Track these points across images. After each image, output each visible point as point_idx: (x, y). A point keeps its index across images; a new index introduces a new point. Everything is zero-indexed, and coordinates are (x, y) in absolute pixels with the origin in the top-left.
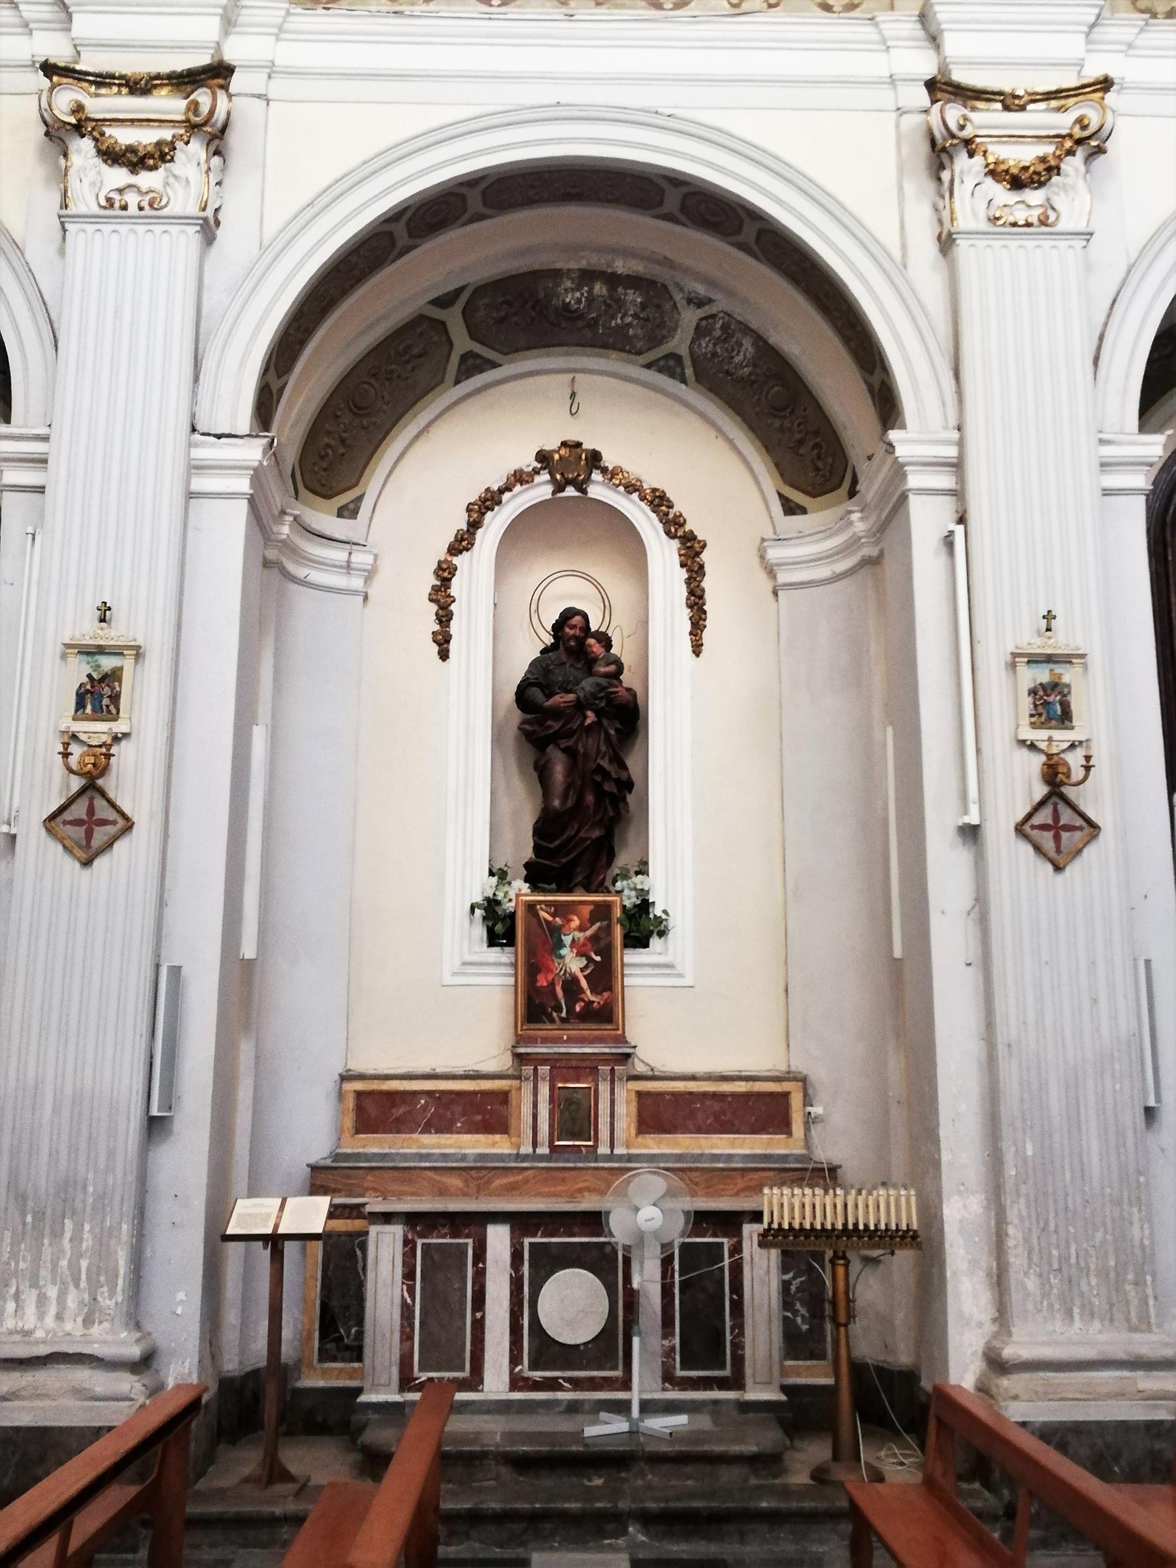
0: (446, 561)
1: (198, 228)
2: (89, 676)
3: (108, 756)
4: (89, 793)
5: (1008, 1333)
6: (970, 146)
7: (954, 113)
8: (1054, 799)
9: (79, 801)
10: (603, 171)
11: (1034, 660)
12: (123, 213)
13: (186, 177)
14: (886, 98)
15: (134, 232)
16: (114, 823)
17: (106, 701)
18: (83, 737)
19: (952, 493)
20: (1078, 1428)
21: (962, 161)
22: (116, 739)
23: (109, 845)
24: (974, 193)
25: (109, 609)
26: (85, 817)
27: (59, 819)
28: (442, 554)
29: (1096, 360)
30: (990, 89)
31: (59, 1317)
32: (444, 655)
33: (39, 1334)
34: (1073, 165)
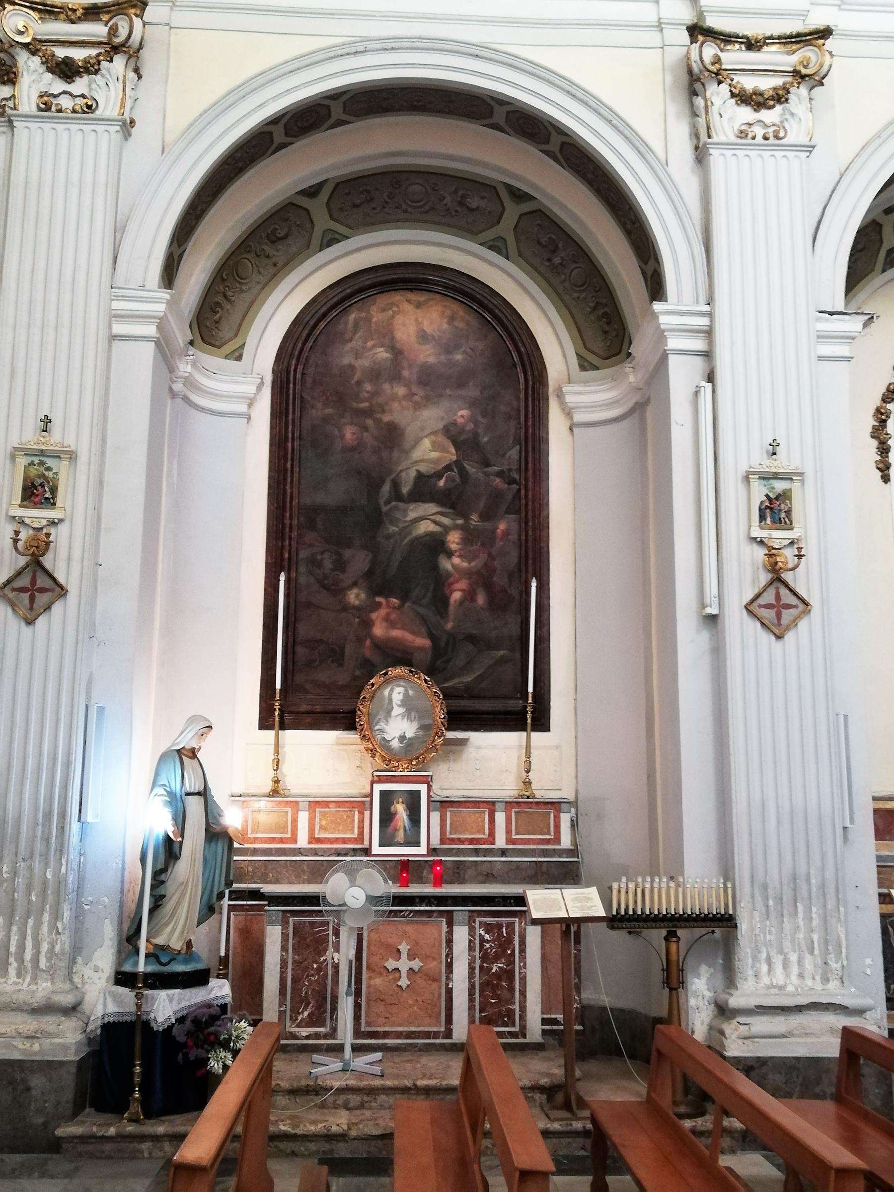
0: (881, 407)
2: (767, 496)
5: (786, 988)
6: (718, 76)
7: (710, 50)
8: (776, 584)
9: (769, 589)
10: (442, 91)
11: (766, 477)
12: (753, 142)
14: (654, 37)
15: (761, 156)
16: (796, 607)
17: (783, 515)
18: (27, 521)
20: (762, 1062)
22: (53, 523)
23: (48, 608)
24: (727, 116)
26: (774, 602)
27: (755, 604)
28: (878, 402)
31: (801, 976)
32: (886, 479)
33: (790, 989)
34: (799, 93)
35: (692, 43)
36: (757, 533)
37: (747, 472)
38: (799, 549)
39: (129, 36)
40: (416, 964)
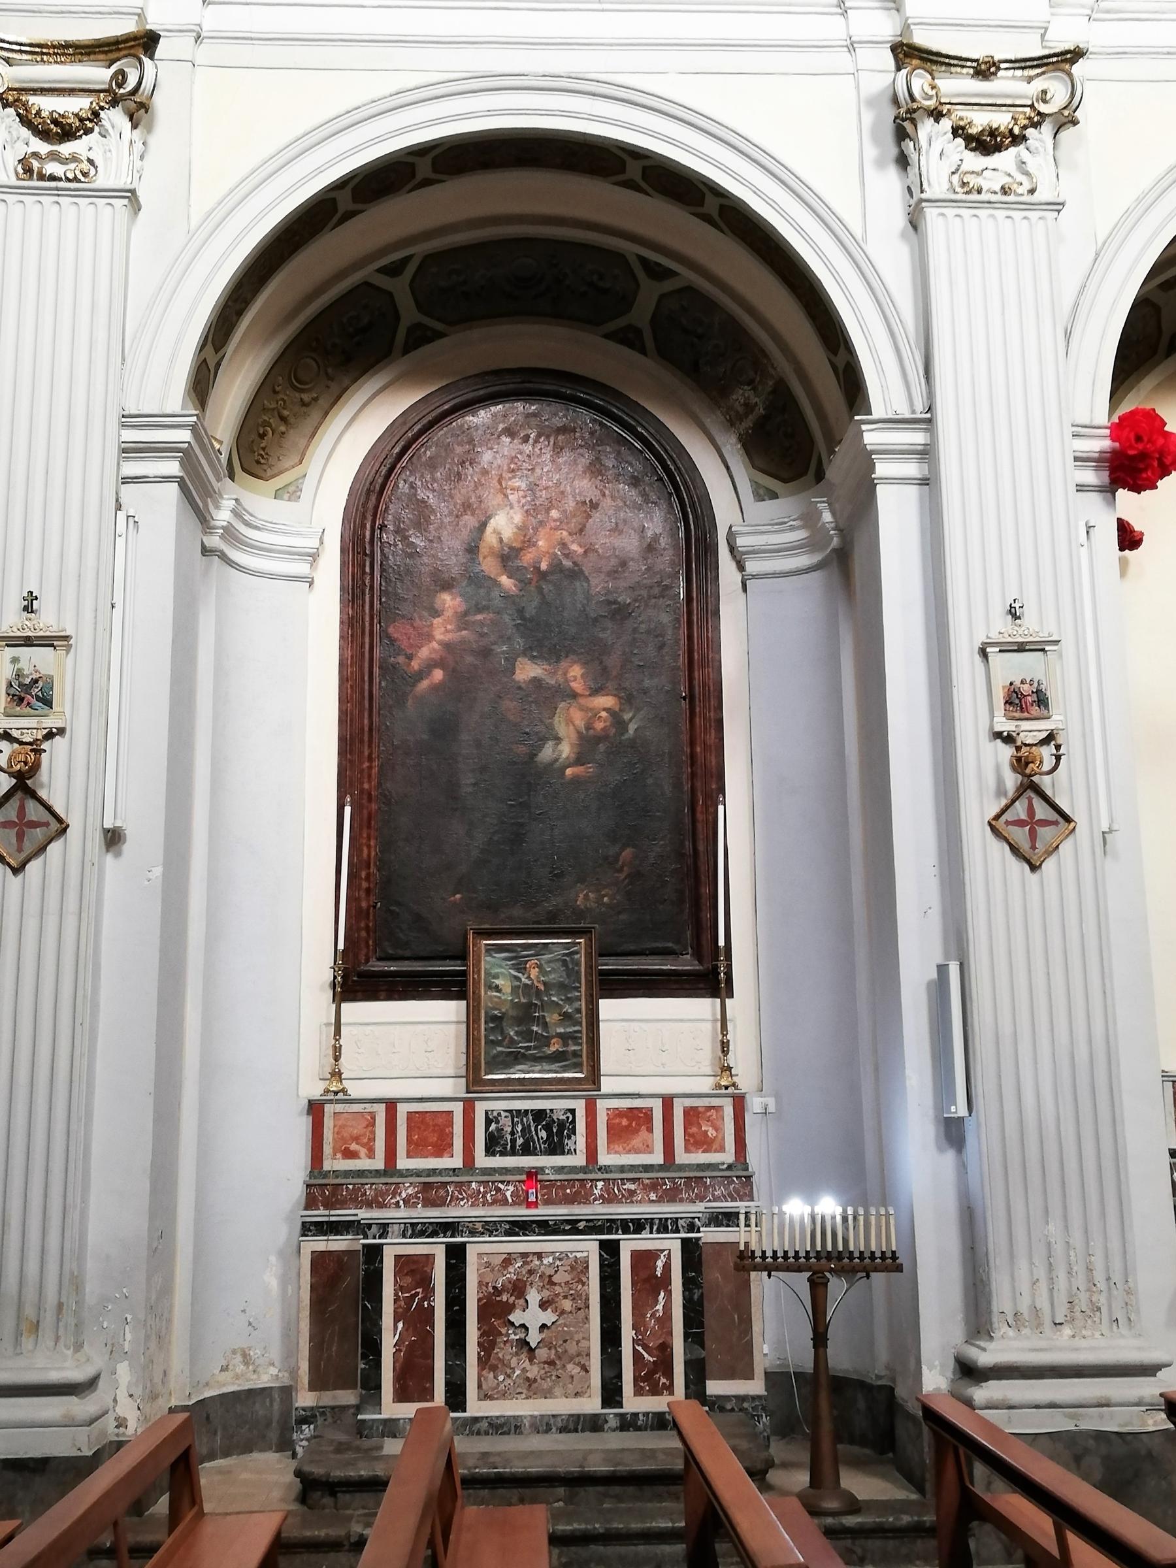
1: (126, 201)
3: (38, 752)
4: (19, 795)
7: (920, 82)
13: (110, 149)
14: (843, 60)
16: (47, 824)
18: (15, 734)
19: (924, 482)
21: (926, 128)
23: (42, 849)
25: (36, 598)
29: (1068, 335)
30: (944, 52)
34: (1040, 137)
35: (899, 69)
36: (1006, 726)
37: (983, 643)
38: (1058, 747)
39: (140, 83)
40: (548, 1317)
